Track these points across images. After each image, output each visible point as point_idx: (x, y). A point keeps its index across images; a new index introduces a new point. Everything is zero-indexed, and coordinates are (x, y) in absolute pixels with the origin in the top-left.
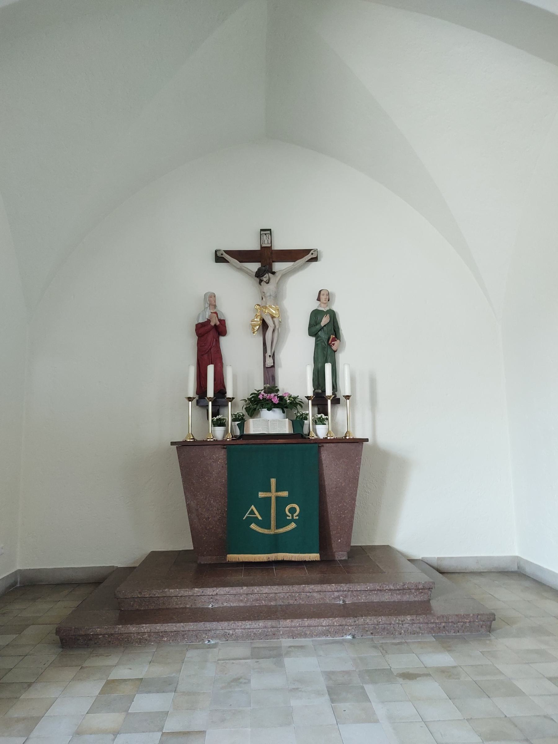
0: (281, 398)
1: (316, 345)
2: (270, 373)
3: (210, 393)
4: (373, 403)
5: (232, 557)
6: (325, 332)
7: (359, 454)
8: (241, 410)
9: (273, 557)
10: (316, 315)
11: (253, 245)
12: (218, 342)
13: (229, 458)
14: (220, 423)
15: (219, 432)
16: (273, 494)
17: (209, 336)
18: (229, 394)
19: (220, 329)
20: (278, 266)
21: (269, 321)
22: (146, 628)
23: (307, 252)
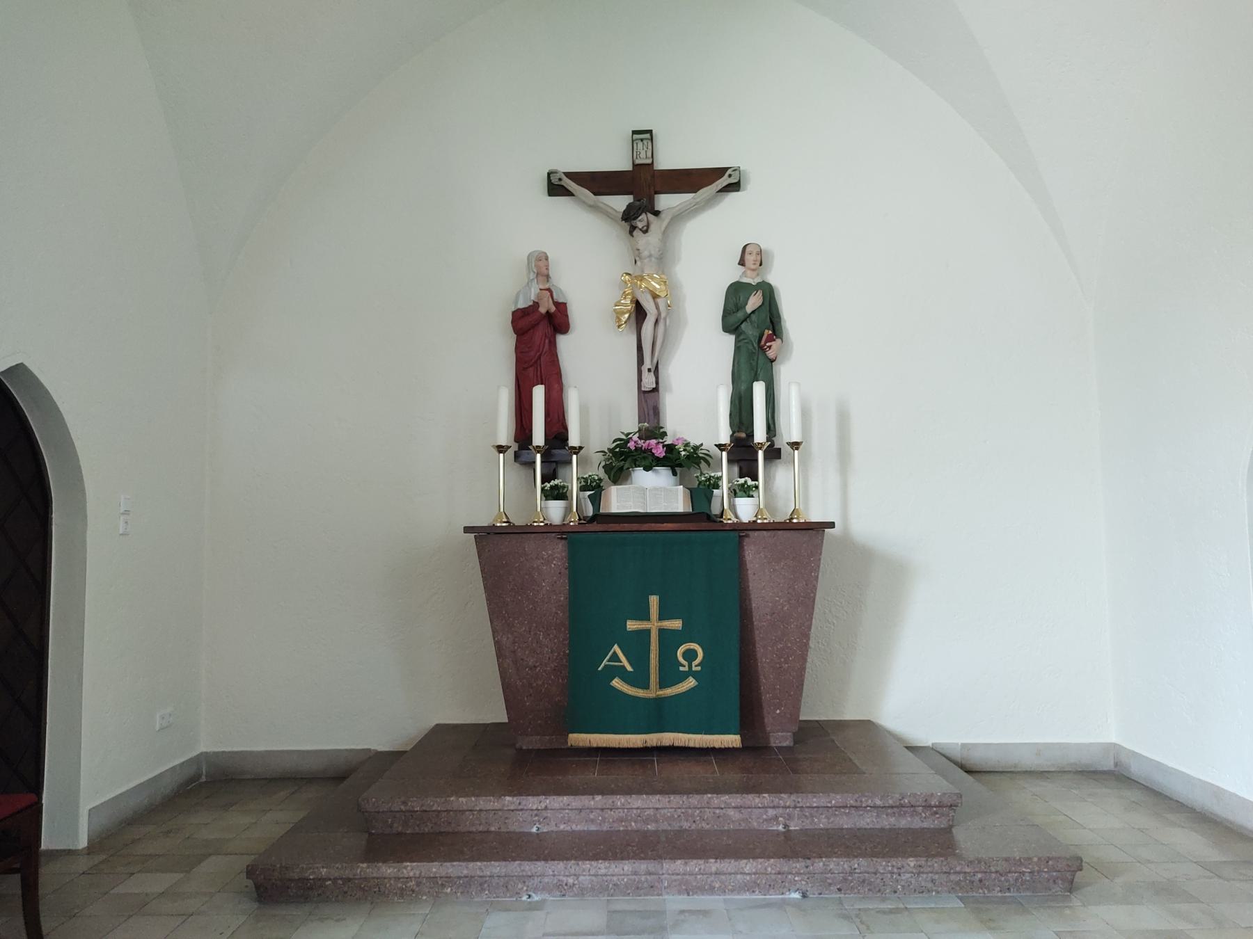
0: (670, 448)
2: (649, 402)
3: (539, 438)
5: (579, 739)
6: (754, 324)
7: (817, 550)
8: (596, 471)
9: (653, 739)
10: (737, 293)
12: (553, 344)
14: (558, 494)
15: (555, 511)
16: (654, 625)
17: (538, 333)
18: (574, 441)
20: (666, 201)
21: (648, 305)
22: (411, 869)
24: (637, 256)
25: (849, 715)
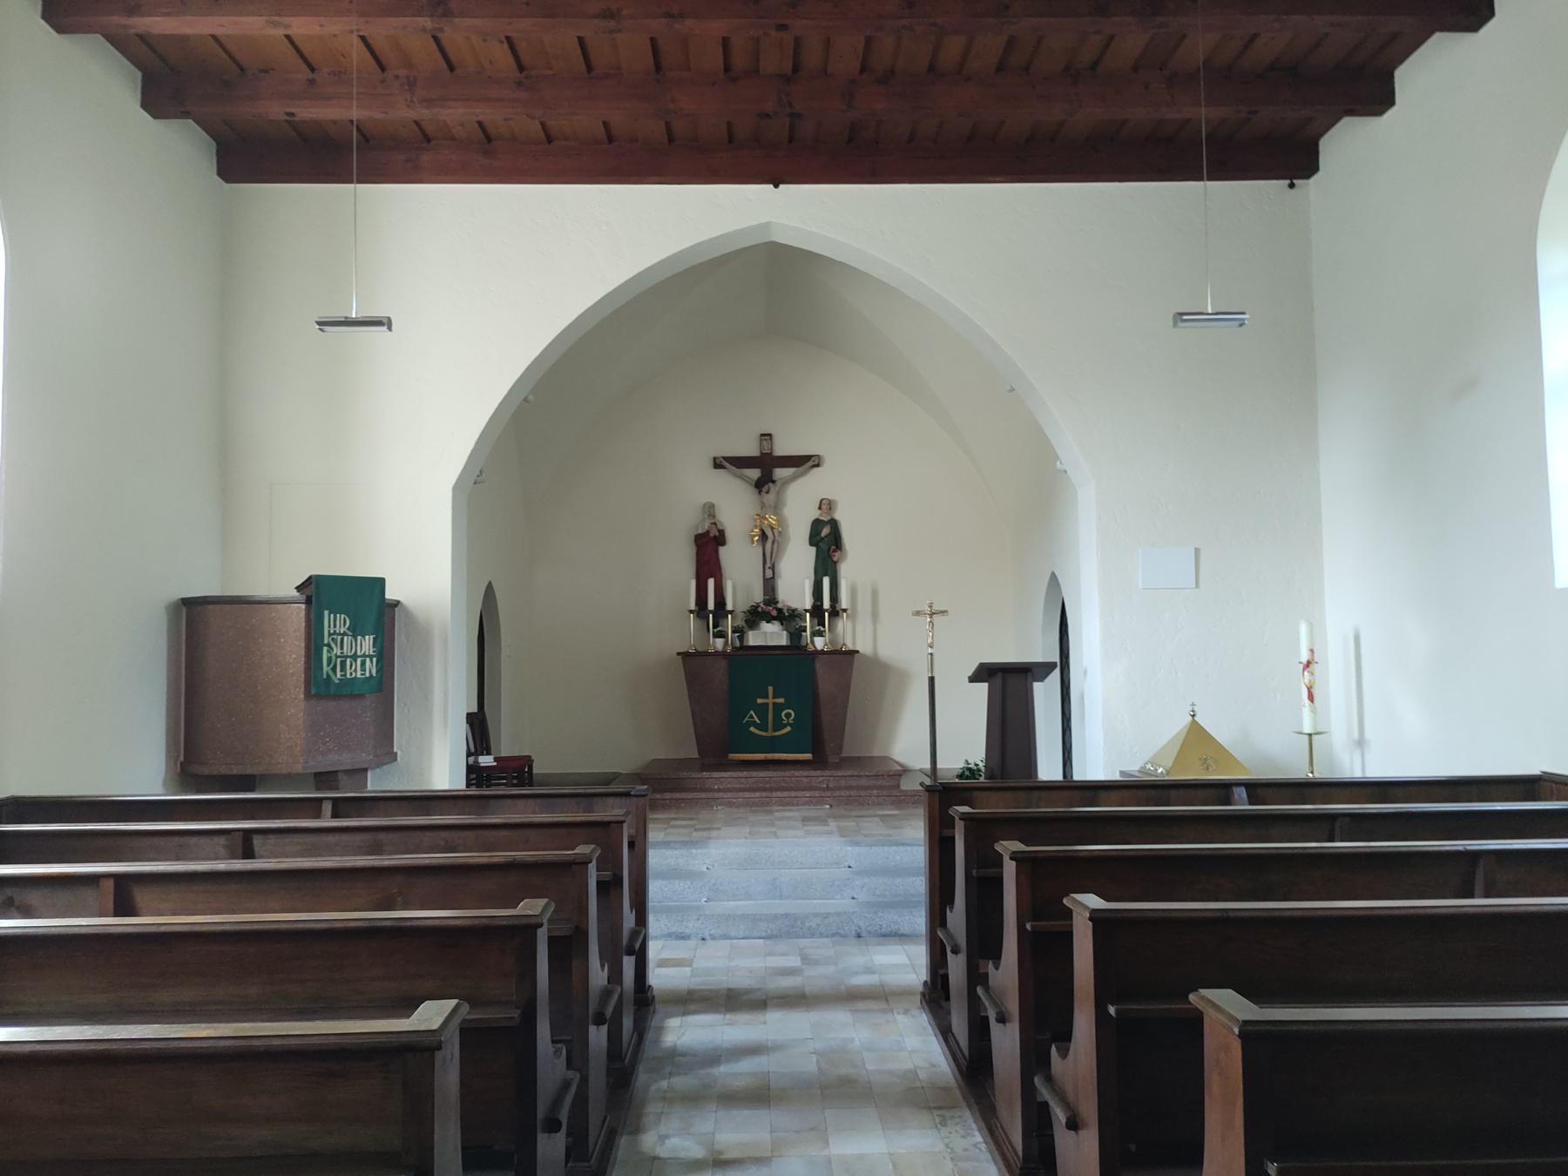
0: (780, 611)
1: (665, 807)
2: (770, 585)
3: (711, 605)
4: (875, 615)
5: (732, 756)
6: (827, 541)
7: (851, 665)
8: (740, 622)
9: (770, 756)
10: (817, 525)
11: (750, 449)
12: (717, 552)
13: (116, 886)
14: (721, 635)
15: (719, 643)
16: (770, 700)
17: (708, 546)
18: (729, 607)
19: (720, 539)
20: (781, 473)
21: (769, 533)
22: (668, 795)
23: (808, 458)
24: (763, 505)
25: (876, 753)
